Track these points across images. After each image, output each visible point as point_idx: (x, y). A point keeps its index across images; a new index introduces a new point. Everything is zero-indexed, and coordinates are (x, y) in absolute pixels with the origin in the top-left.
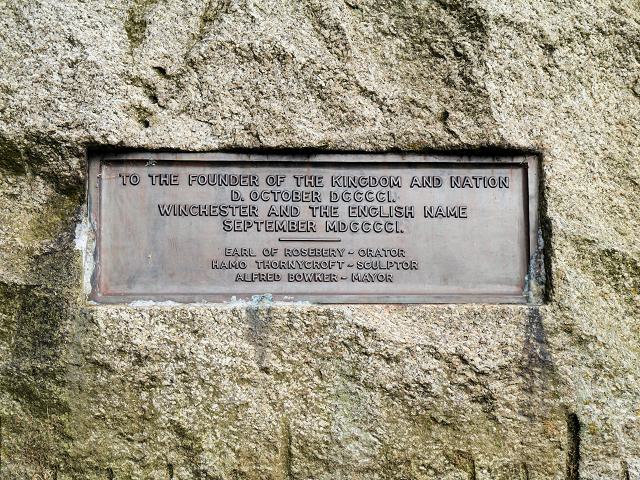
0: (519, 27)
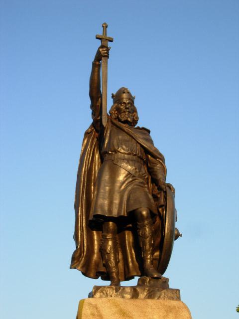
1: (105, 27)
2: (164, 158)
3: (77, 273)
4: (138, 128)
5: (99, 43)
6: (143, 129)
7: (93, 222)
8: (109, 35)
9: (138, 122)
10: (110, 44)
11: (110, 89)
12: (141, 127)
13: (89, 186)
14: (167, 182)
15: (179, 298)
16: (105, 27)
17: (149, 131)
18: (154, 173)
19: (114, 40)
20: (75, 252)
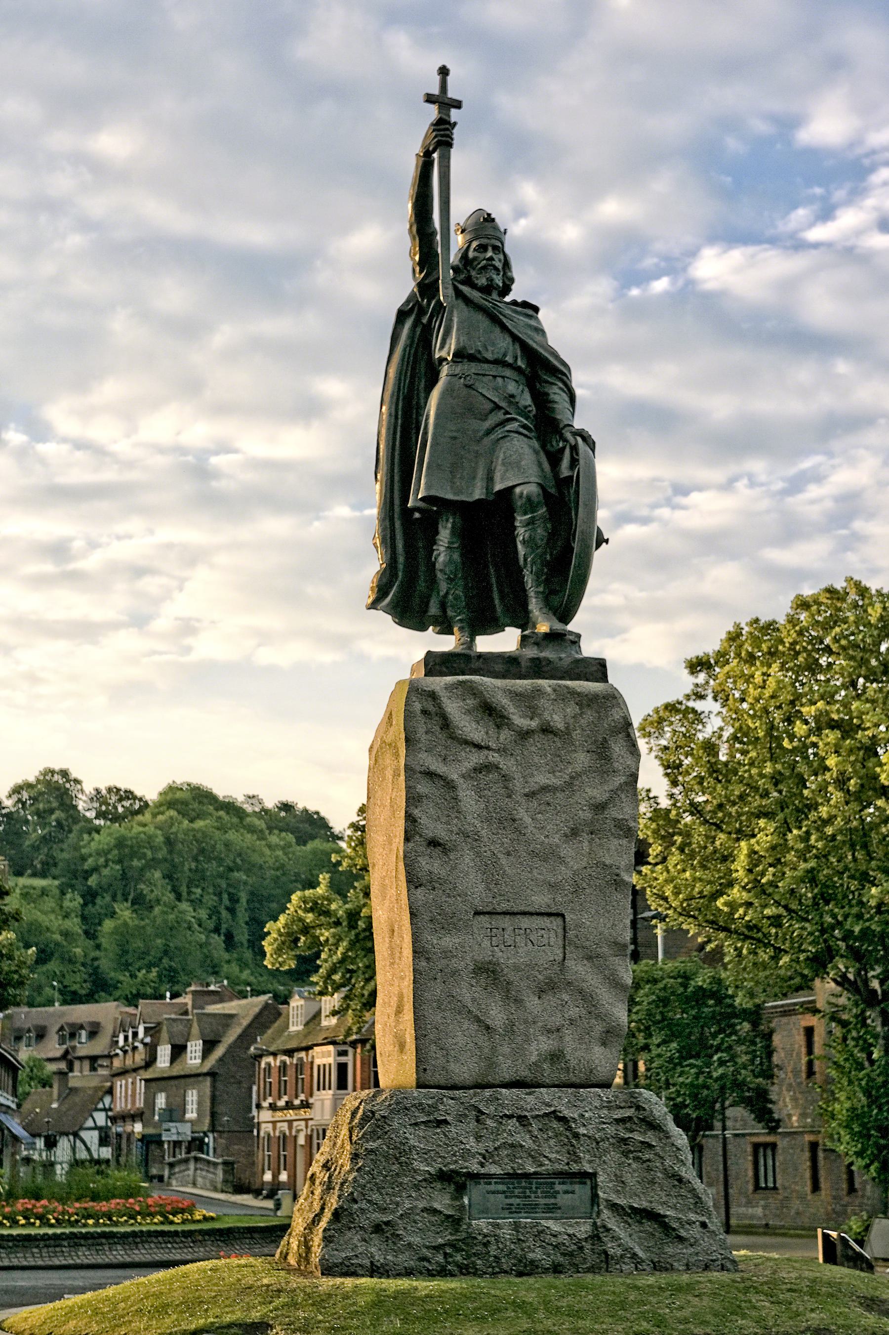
0: (589, 1137)
1: (444, 72)
2: (594, 443)
3: (384, 620)
4: (514, 303)
5: (433, 113)
6: (525, 305)
7: (406, 529)
8: (452, 94)
9: (513, 287)
10: (455, 115)
11: (462, 208)
12: (519, 300)
13: (76, 1241)
14: (577, 424)
15: (604, 678)
16: (444, 72)
17: (536, 309)
18: (550, 405)
19: (464, 104)
20: (382, 574)
